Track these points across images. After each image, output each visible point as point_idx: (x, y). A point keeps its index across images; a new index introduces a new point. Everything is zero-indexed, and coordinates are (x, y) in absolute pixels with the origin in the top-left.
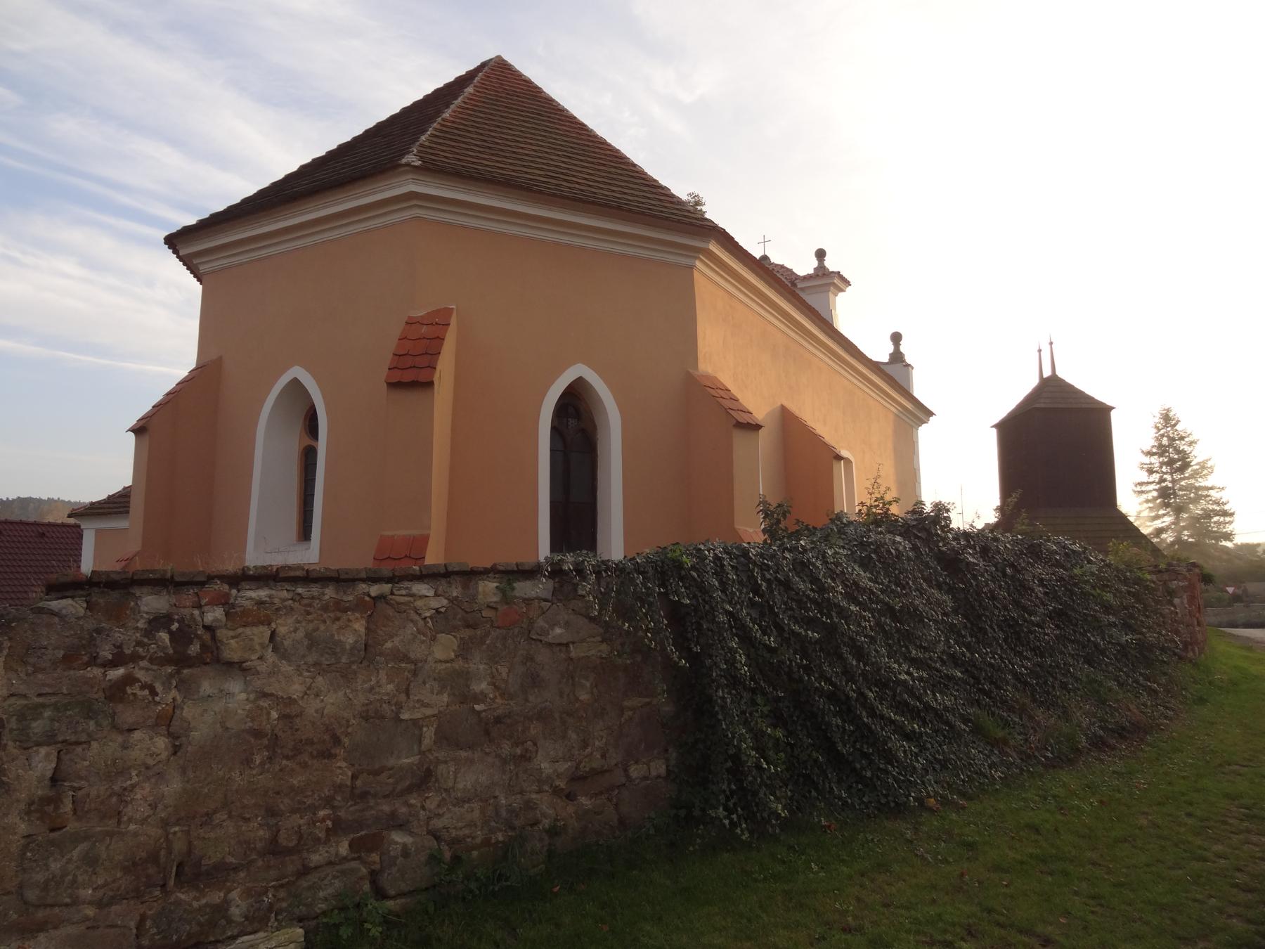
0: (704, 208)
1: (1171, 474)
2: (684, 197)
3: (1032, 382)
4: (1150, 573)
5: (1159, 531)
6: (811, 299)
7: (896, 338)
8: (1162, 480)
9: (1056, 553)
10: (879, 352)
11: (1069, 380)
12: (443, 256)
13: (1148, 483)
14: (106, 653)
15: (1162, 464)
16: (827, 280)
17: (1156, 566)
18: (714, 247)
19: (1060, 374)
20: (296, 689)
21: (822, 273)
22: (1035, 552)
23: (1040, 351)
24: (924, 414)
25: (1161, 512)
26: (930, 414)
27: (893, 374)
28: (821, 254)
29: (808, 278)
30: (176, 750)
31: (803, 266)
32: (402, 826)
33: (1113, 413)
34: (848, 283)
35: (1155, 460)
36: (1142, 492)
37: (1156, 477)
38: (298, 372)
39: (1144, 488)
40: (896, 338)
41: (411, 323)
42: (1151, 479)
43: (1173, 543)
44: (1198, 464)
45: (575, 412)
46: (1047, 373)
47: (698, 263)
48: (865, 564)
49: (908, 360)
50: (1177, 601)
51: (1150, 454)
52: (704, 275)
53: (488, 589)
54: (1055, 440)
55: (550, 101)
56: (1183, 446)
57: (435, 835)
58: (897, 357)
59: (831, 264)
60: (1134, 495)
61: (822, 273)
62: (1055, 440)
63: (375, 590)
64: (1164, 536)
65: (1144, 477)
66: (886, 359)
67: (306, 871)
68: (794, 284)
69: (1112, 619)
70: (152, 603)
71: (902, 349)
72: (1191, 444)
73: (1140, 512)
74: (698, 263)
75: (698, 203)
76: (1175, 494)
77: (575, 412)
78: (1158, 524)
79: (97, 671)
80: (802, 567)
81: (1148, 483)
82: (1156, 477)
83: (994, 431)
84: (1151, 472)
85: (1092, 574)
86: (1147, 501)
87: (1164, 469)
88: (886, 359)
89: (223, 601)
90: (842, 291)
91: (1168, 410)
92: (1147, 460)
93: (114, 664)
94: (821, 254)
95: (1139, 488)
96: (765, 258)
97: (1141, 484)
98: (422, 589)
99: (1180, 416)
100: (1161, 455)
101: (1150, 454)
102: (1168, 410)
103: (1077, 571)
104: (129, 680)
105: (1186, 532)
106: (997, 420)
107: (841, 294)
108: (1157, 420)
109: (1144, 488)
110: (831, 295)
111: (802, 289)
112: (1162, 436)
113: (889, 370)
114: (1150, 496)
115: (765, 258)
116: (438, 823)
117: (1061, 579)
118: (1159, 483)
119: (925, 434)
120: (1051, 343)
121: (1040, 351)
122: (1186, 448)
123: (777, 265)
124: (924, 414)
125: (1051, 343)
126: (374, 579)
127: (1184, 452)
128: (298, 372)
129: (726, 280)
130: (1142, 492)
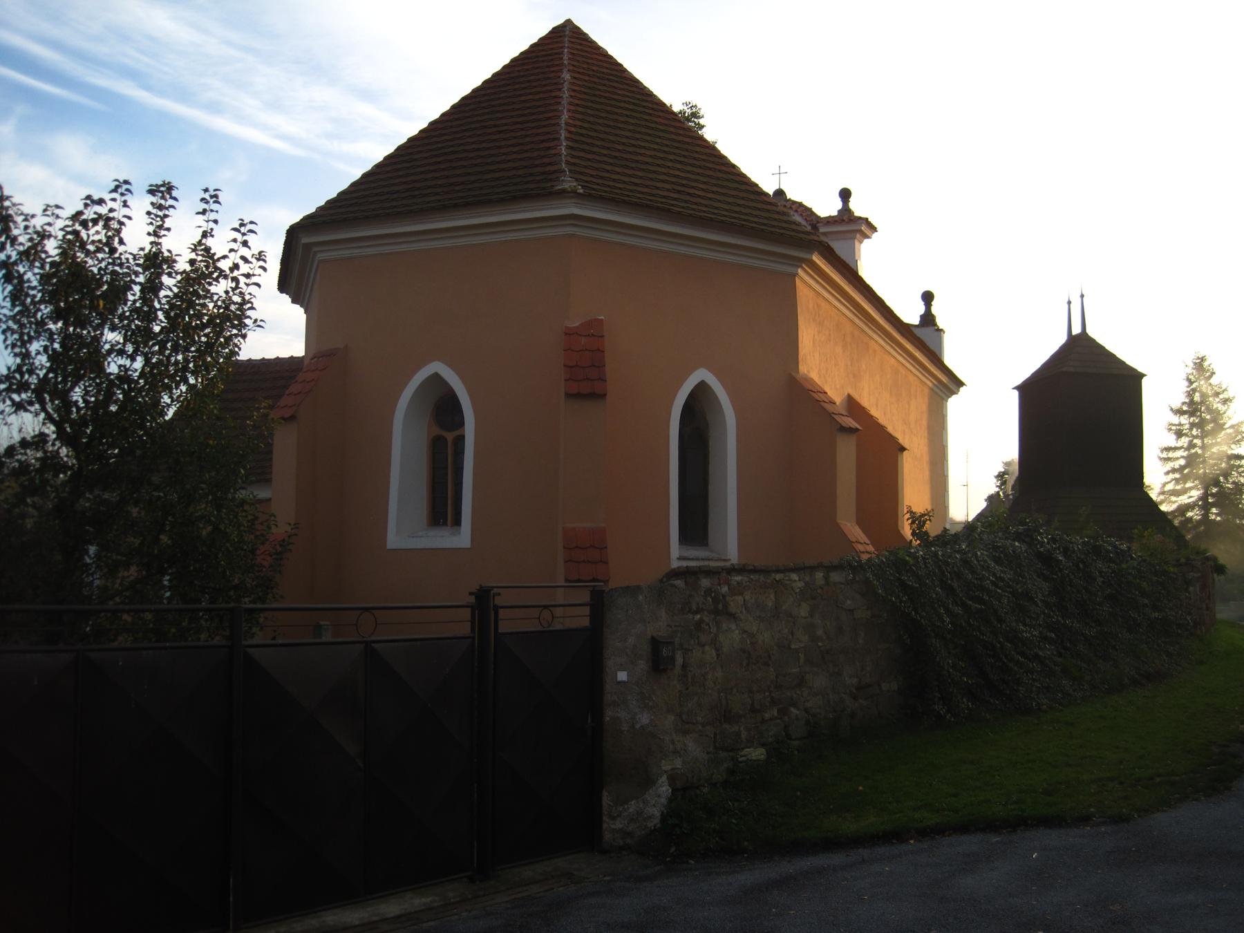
0: (702, 121)
1: (1202, 438)
2: (676, 108)
3: (1056, 340)
4: (1174, 566)
5: (1182, 510)
6: (838, 247)
7: (928, 297)
8: (1191, 445)
9: (1109, 552)
10: (911, 313)
11: (1101, 340)
12: (573, 260)
13: (1175, 449)
14: (694, 607)
15: (1192, 425)
16: (851, 225)
17: (1178, 560)
18: (817, 259)
19: (1091, 332)
20: (754, 629)
21: (846, 215)
22: (1097, 551)
23: (1069, 303)
24: (954, 383)
25: (1189, 485)
26: (960, 384)
27: (923, 339)
28: (845, 194)
29: (829, 221)
30: (718, 656)
31: (827, 207)
32: (794, 705)
33: (1144, 381)
34: (874, 229)
35: (1185, 420)
36: (1168, 459)
37: (1184, 441)
38: (437, 367)
39: (1171, 455)
40: (928, 297)
41: (569, 333)
42: (1179, 444)
43: (1199, 522)
44: (1232, 427)
45: (698, 412)
46: (1076, 330)
47: (800, 271)
48: (997, 561)
49: (940, 323)
50: (1191, 589)
51: (1179, 412)
52: (805, 283)
53: (819, 575)
54: (1081, 402)
55: (599, 48)
56: (1217, 405)
57: (806, 710)
58: (928, 319)
59: (858, 207)
60: (1161, 463)
61: (846, 215)
62: (1081, 402)
63: (778, 577)
64: (1189, 514)
65: (1171, 440)
66: (915, 320)
67: (763, 721)
68: (815, 227)
69: (1146, 601)
70: (705, 582)
71: (934, 310)
72: (1226, 401)
73: (1164, 485)
74: (800, 271)
75: (695, 115)
76: (1204, 462)
77: (698, 412)
78: (1184, 500)
79: (691, 616)
80: (966, 562)
81: (1175, 449)
82: (1184, 441)
83: (1016, 393)
84: (1179, 434)
85: (1133, 568)
86: (1174, 471)
87: (1194, 432)
88: (915, 320)
89: (727, 583)
90: (868, 237)
91: (1203, 359)
92: (1175, 419)
93: (696, 613)
94: (845, 194)
95: (1164, 455)
96: (780, 193)
97: (1168, 449)
98: (794, 576)
99: (1215, 367)
100: (1192, 413)
101: (1179, 412)
102: (1203, 359)
103: (1124, 566)
104: (701, 621)
105: (1214, 510)
106: (1019, 380)
107: (866, 241)
108: (1190, 370)
109: (1171, 455)
110: (857, 243)
111: (825, 234)
112: (1194, 390)
113: (918, 332)
114: (1177, 464)
115: (780, 193)
116: (809, 705)
117: (1114, 572)
118: (1188, 449)
119: (954, 405)
120: (1082, 296)
121: (1069, 303)
122: (1220, 406)
123: (794, 202)
124: (954, 383)
125: (1082, 296)
126: (778, 571)
127: (1217, 412)
128: (437, 367)
129: (817, 282)
130: (1168, 459)
